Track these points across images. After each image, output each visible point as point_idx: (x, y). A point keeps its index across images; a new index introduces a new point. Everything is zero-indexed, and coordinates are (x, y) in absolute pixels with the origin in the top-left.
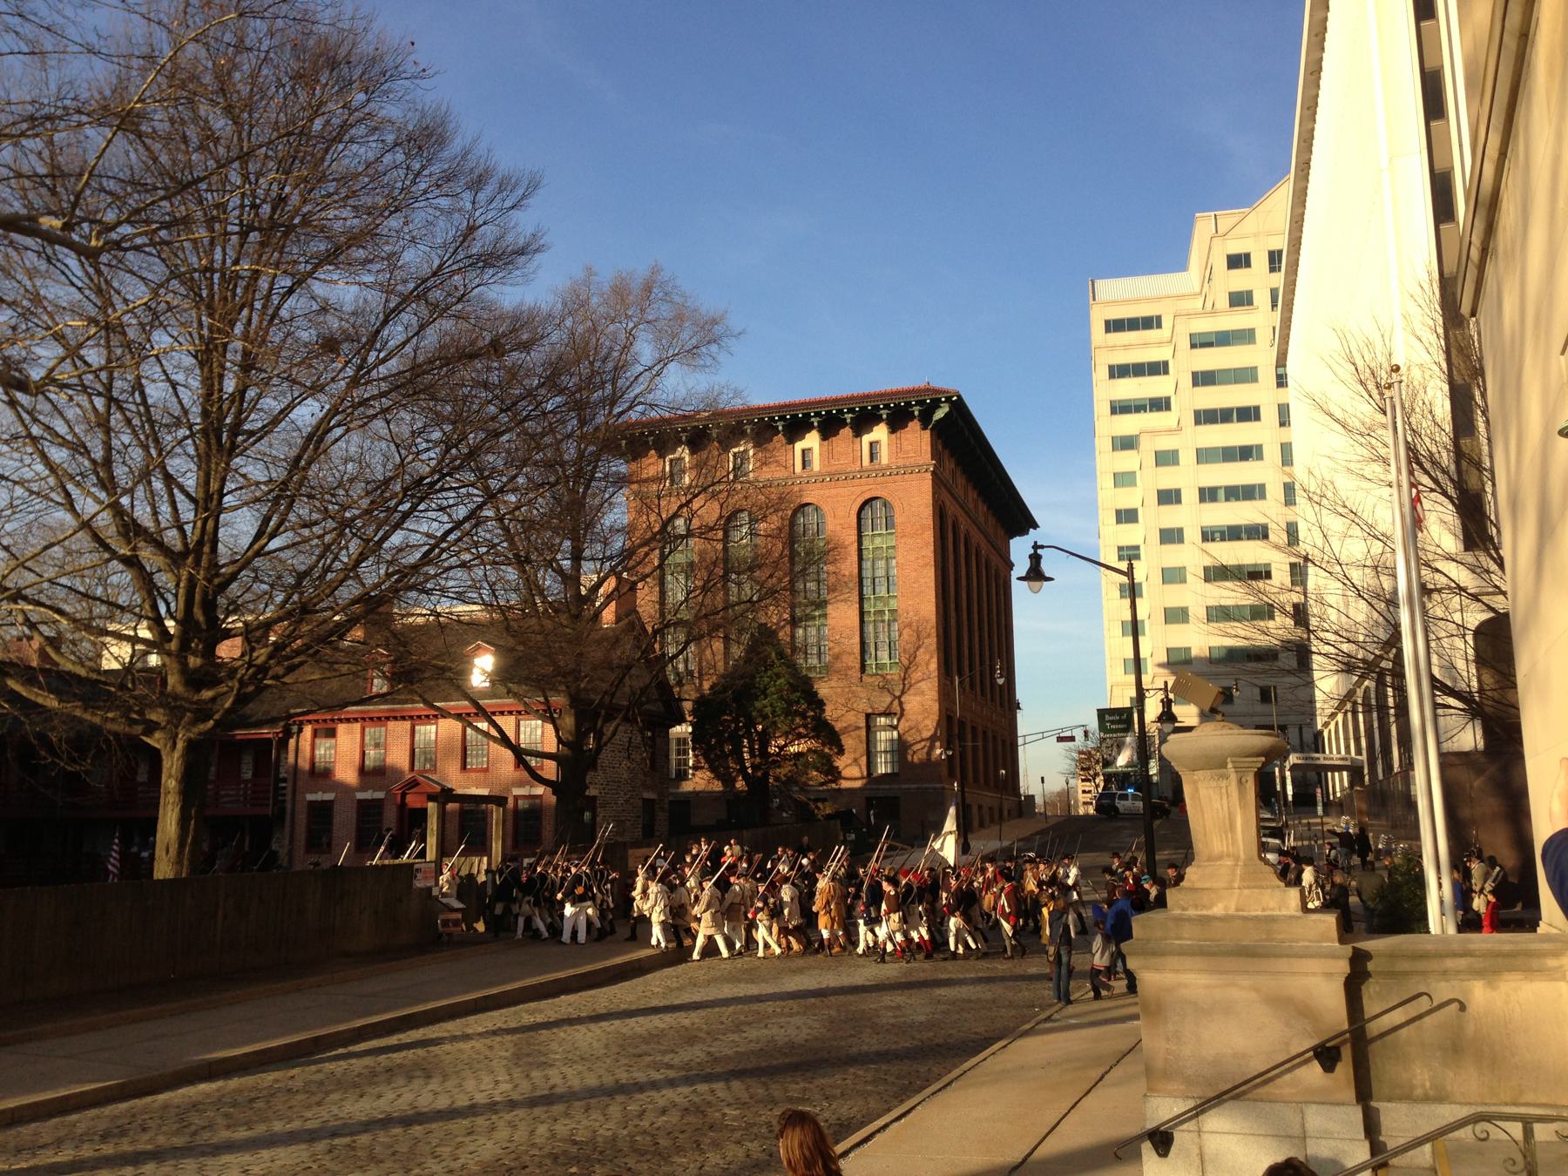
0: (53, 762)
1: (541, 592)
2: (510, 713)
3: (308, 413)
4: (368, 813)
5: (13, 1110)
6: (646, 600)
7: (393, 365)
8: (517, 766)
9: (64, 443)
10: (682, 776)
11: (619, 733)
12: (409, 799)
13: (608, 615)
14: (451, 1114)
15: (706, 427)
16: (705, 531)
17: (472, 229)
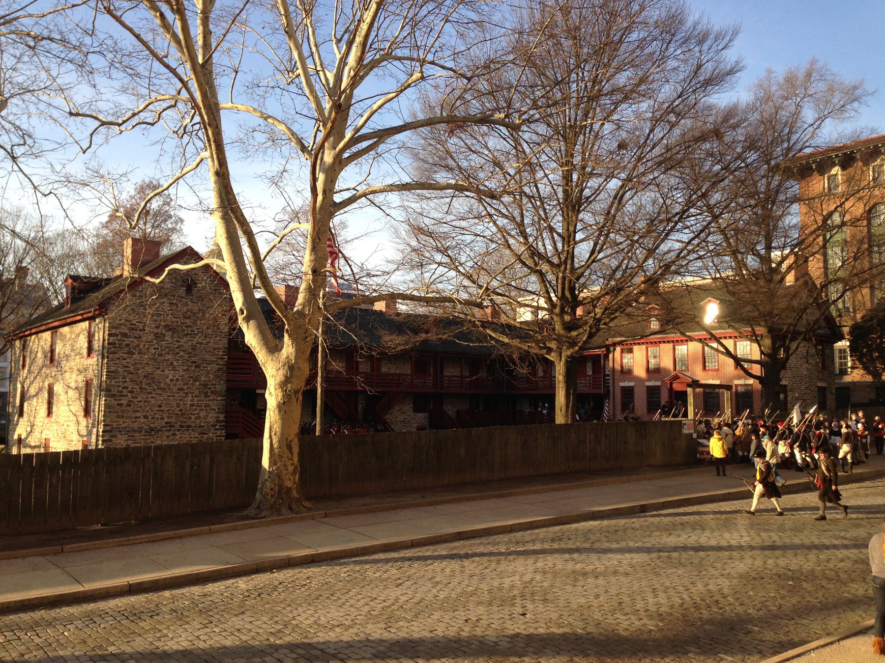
0: (515, 369)
1: (745, 265)
2: (730, 337)
3: (614, 184)
4: (652, 392)
5: (511, 525)
6: (815, 267)
7: (657, 151)
8: (736, 368)
9: (506, 217)
10: (844, 372)
11: (801, 348)
12: (674, 385)
13: (790, 279)
14: (719, 548)
15: (852, 152)
16: (854, 222)
17: (699, 67)
